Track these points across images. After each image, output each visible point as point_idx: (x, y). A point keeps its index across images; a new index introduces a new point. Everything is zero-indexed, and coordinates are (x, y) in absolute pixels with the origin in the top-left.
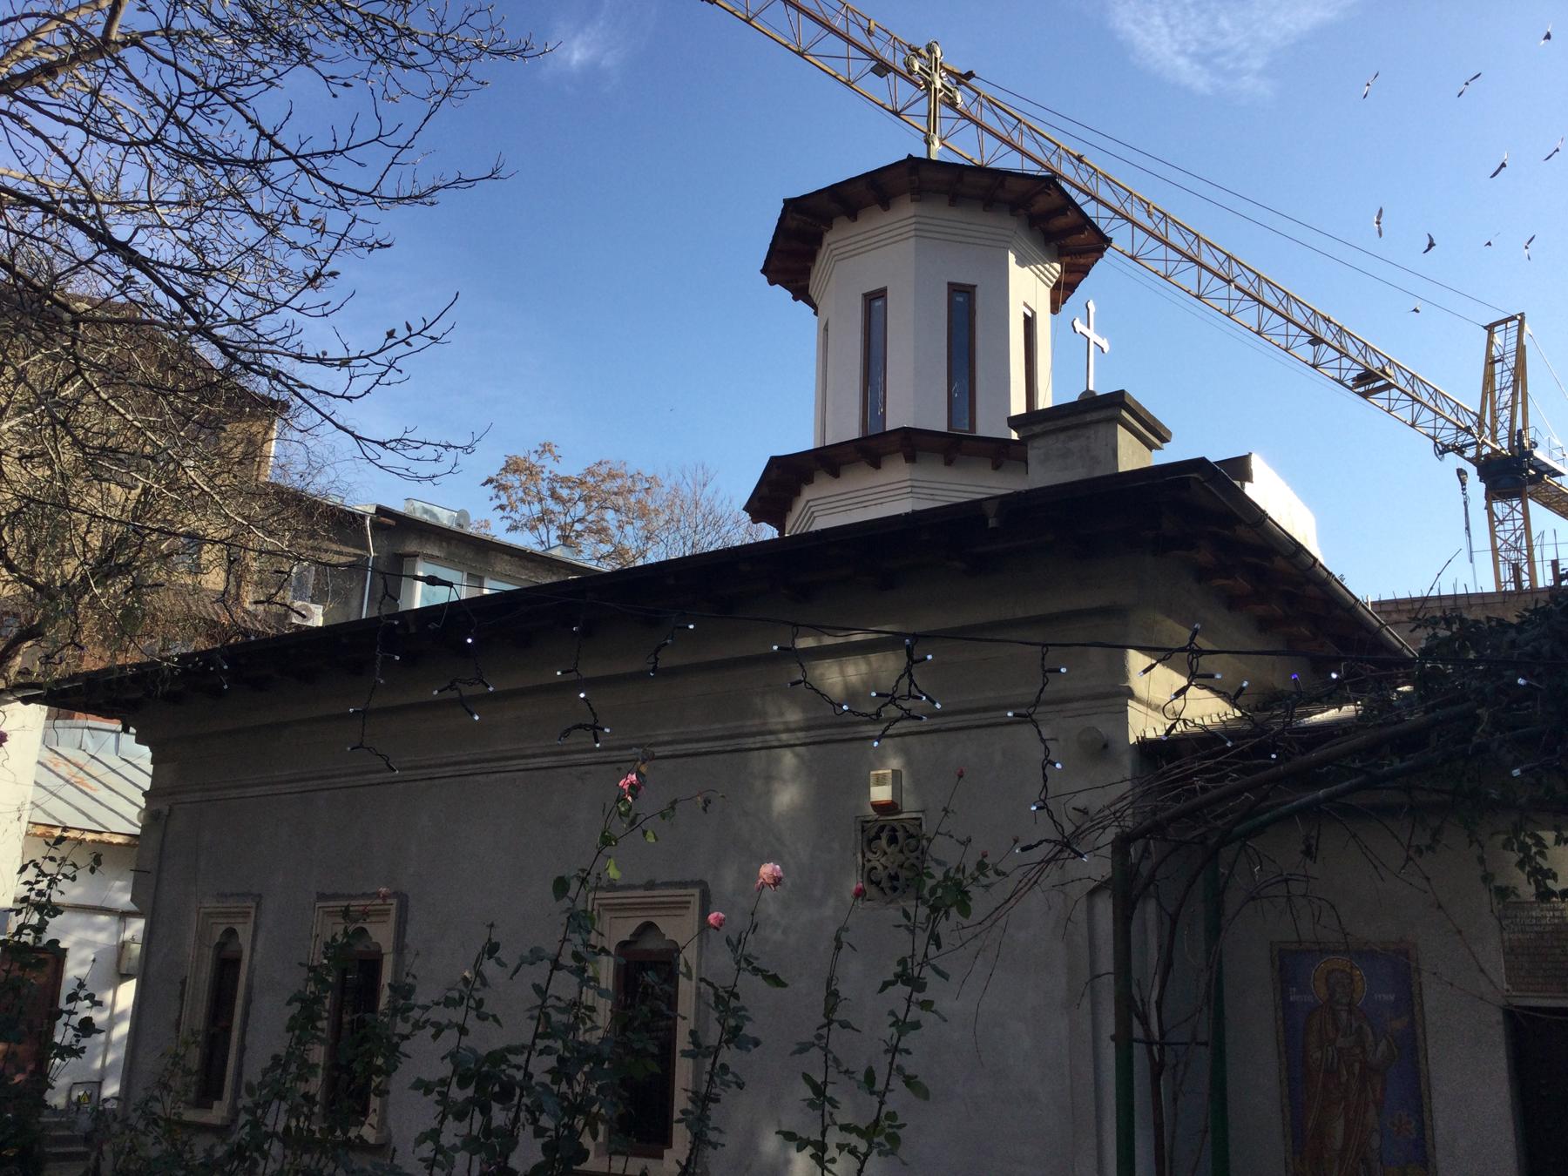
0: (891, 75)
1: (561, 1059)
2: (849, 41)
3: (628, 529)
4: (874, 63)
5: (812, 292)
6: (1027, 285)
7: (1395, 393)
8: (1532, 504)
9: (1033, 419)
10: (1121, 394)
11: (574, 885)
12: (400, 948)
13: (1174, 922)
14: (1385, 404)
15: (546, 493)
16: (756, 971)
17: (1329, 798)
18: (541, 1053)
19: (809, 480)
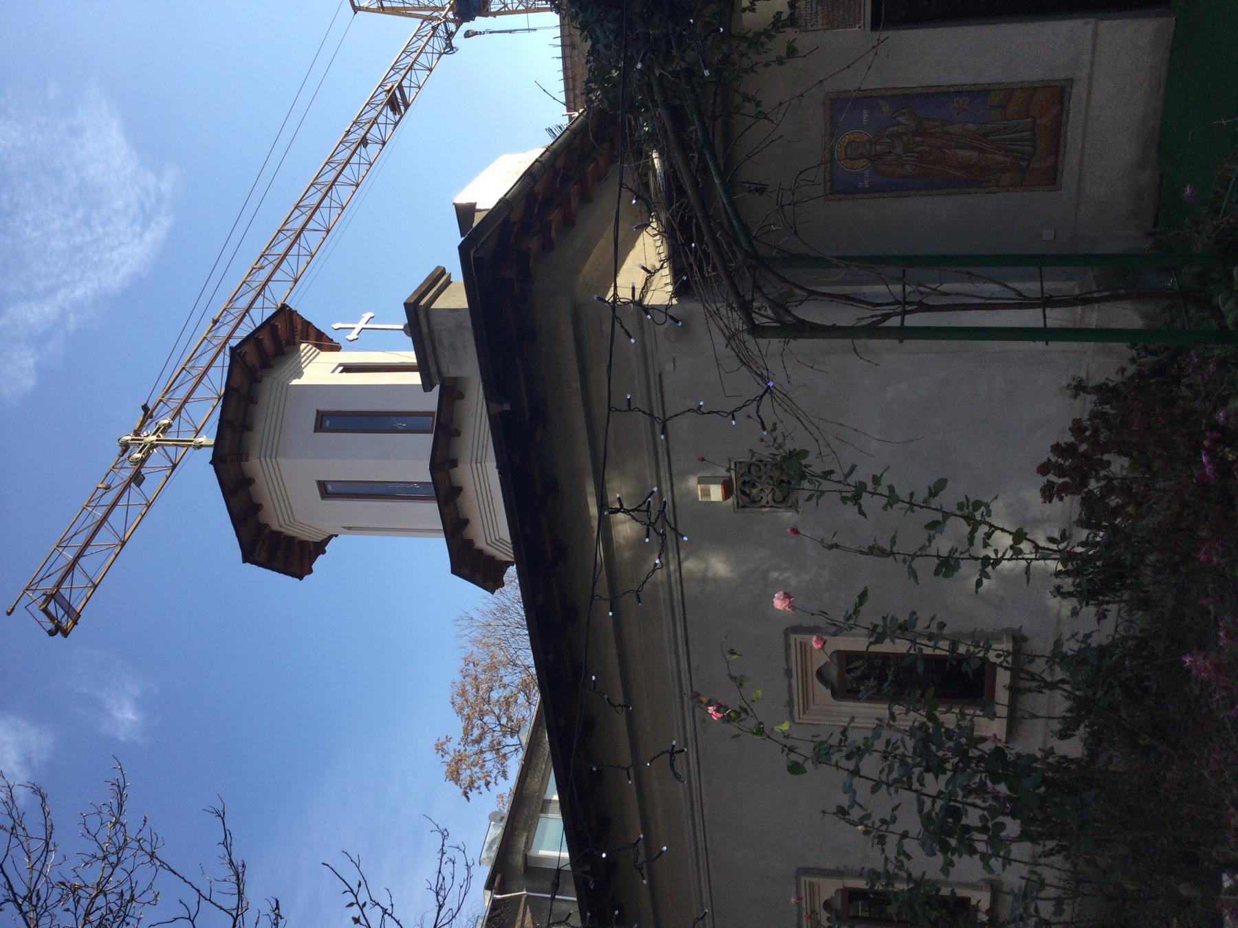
0: (143, 471)
1: (927, 770)
2: (114, 504)
3: (506, 680)
5: (318, 539)
6: (318, 370)
7: (405, 83)
9: (422, 366)
10: (406, 305)
11: (793, 757)
12: (838, 874)
13: (813, 293)
15: (476, 748)
16: (856, 612)
17: (722, 175)
18: (922, 785)
19: (471, 542)
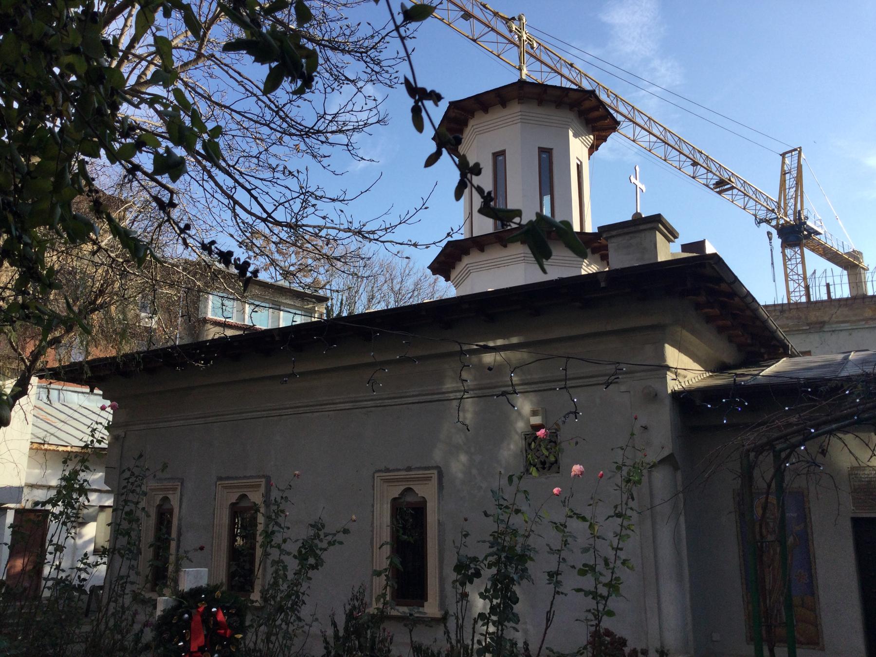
4: (463, 13)
6: (578, 147)
7: (735, 191)
8: (806, 250)
10: (659, 215)
14: (729, 197)
19: (467, 253)
